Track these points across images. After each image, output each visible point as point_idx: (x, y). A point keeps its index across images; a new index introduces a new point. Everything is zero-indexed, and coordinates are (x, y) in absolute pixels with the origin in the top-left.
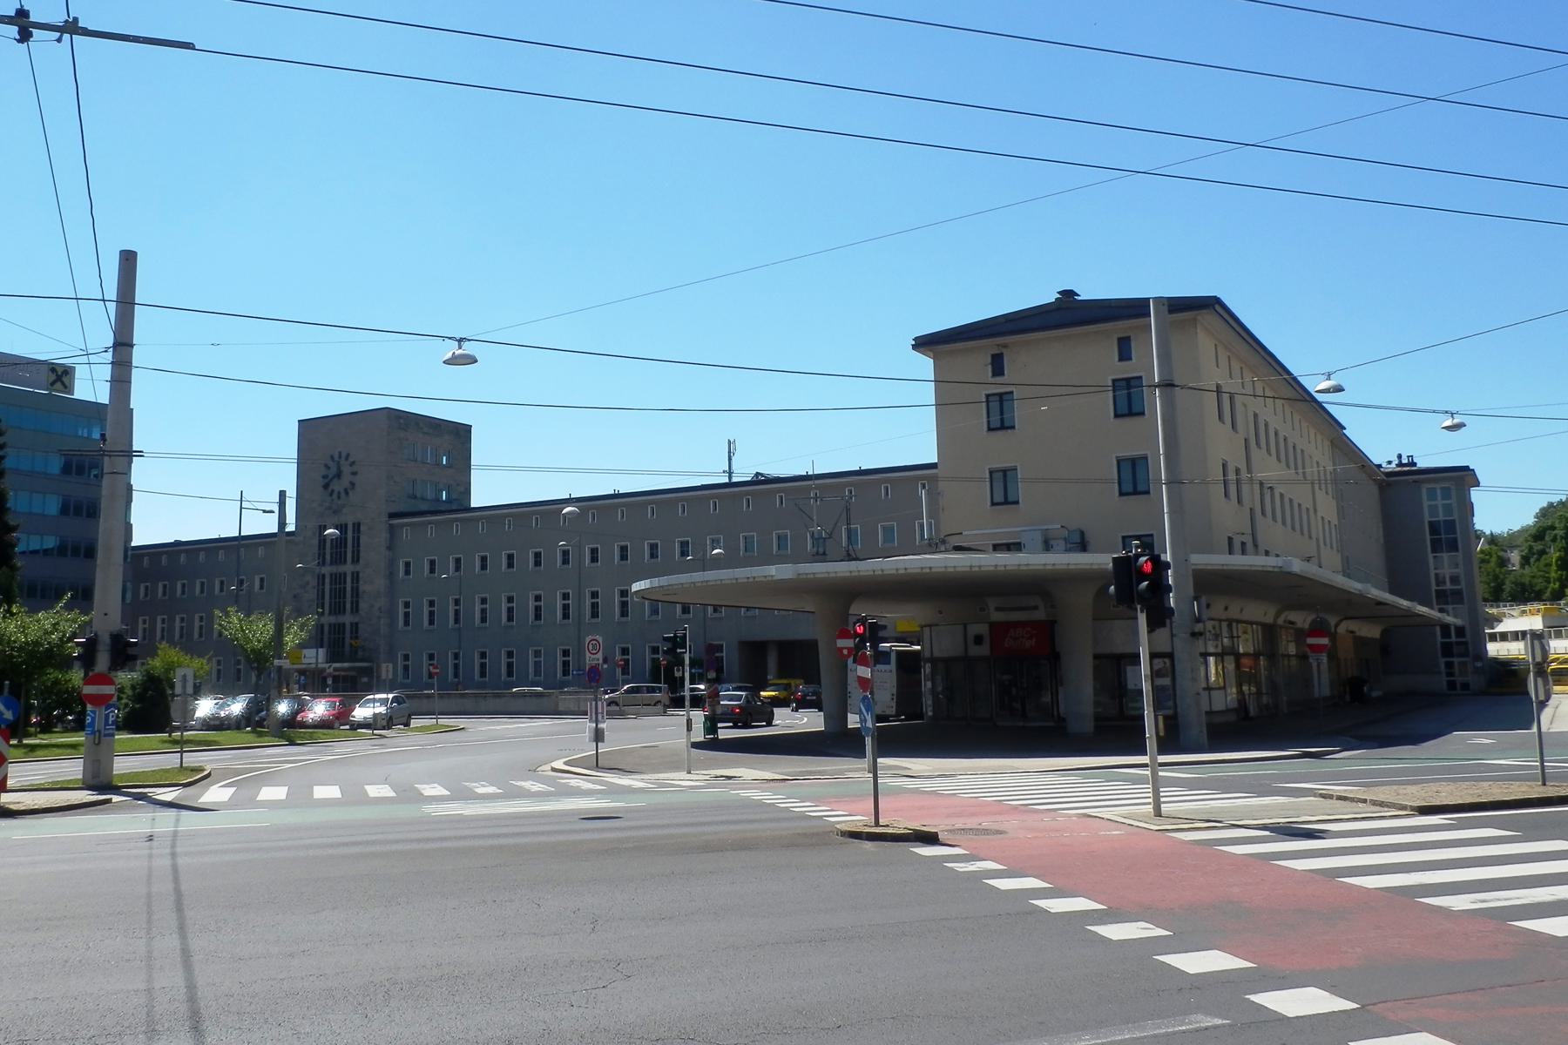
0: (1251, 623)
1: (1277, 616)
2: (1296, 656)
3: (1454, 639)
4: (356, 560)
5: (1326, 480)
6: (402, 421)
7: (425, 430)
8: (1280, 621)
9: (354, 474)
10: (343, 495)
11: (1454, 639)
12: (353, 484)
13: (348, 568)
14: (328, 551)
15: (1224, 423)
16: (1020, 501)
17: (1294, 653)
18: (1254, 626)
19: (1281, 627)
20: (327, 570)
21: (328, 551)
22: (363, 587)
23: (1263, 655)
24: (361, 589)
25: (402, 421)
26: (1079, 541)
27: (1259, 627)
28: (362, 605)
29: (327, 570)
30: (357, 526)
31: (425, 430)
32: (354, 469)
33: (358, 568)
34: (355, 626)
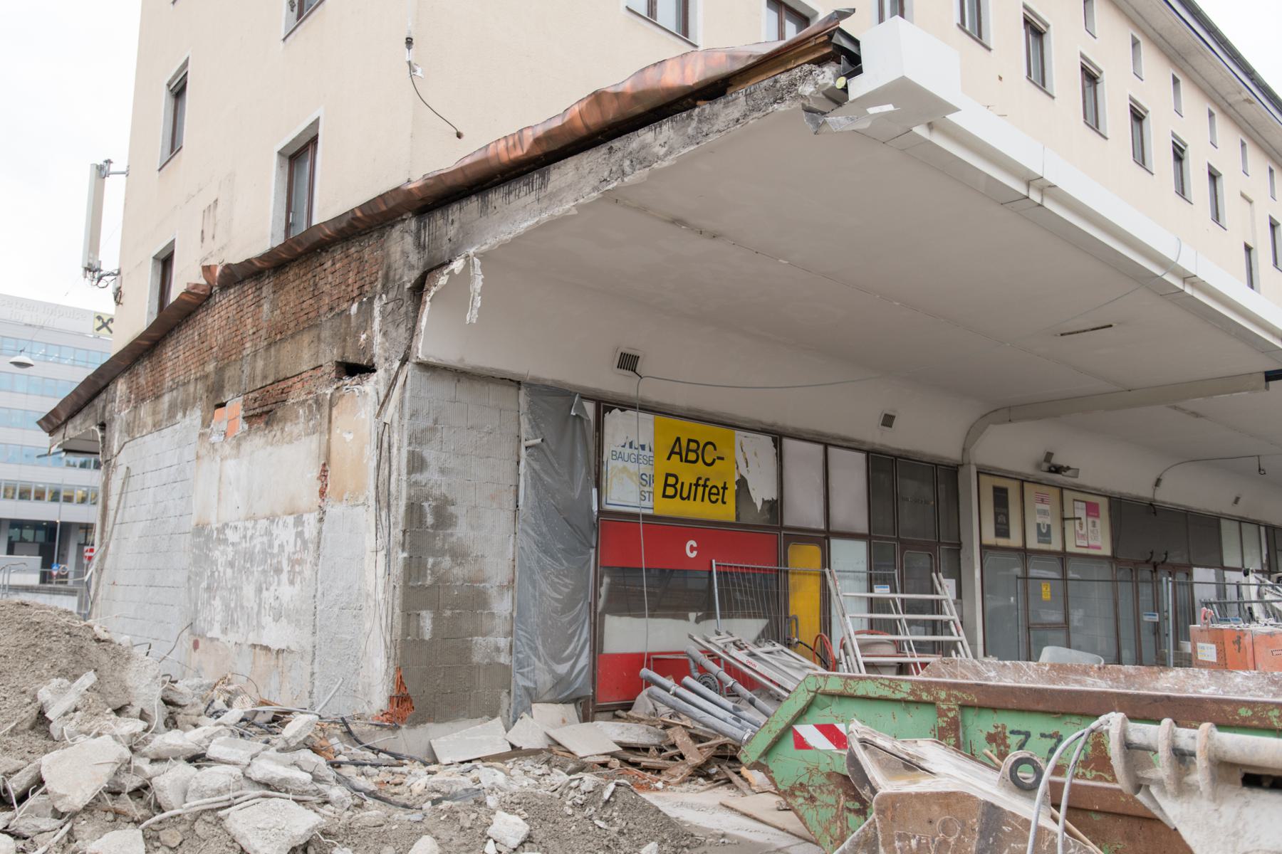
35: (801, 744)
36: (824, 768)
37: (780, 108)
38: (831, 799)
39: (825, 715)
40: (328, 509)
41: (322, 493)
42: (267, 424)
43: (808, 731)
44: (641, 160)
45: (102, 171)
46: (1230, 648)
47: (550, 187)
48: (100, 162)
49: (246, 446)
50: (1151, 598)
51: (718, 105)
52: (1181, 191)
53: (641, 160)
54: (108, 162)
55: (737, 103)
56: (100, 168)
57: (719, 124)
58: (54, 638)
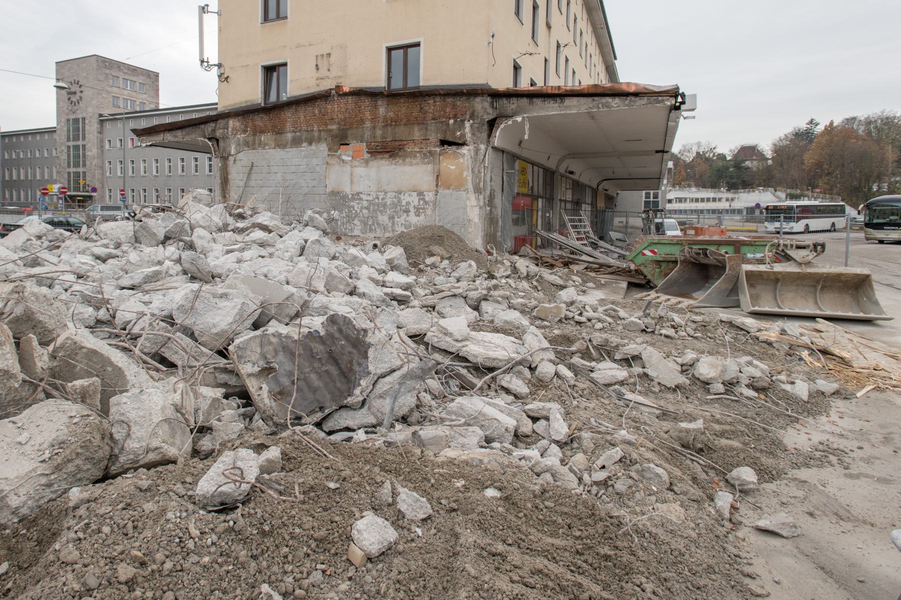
0: (533, 164)
1: (560, 162)
2: (572, 202)
3: (652, 199)
4: (84, 138)
5: (537, 211)
6: (107, 64)
7: (126, 71)
8: (562, 170)
9: (82, 92)
10: (77, 103)
11: (652, 199)
12: (81, 98)
13: (80, 143)
14: (71, 133)
15: (532, 79)
16: (289, 16)
17: (570, 200)
18: (536, 168)
19: (562, 176)
20: (71, 144)
21: (71, 133)
22: (88, 153)
23: (542, 198)
24: (87, 154)
25: (107, 64)
26: (530, 199)
27: (541, 170)
28: (88, 163)
29: (71, 144)
30: (84, 119)
31: (126, 71)
32: (82, 89)
33: (84, 143)
34: (84, 173)
35: (644, 254)
36: (650, 259)
37: (658, 105)
38: (353, 276)
39: (651, 248)
40: (440, 191)
41: (437, 185)
42: (390, 157)
43: (647, 252)
44: (607, 106)
45: (203, 9)
46: (699, 231)
47: (565, 104)
48: (203, 5)
49: (371, 163)
50: (87, 127)
51: (637, 99)
52: (517, 13)
53: (604, 105)
54: (207, 5)
55: (645, 100)
56: (203, 8)
57: (638, 104)
58: (258, 234)
